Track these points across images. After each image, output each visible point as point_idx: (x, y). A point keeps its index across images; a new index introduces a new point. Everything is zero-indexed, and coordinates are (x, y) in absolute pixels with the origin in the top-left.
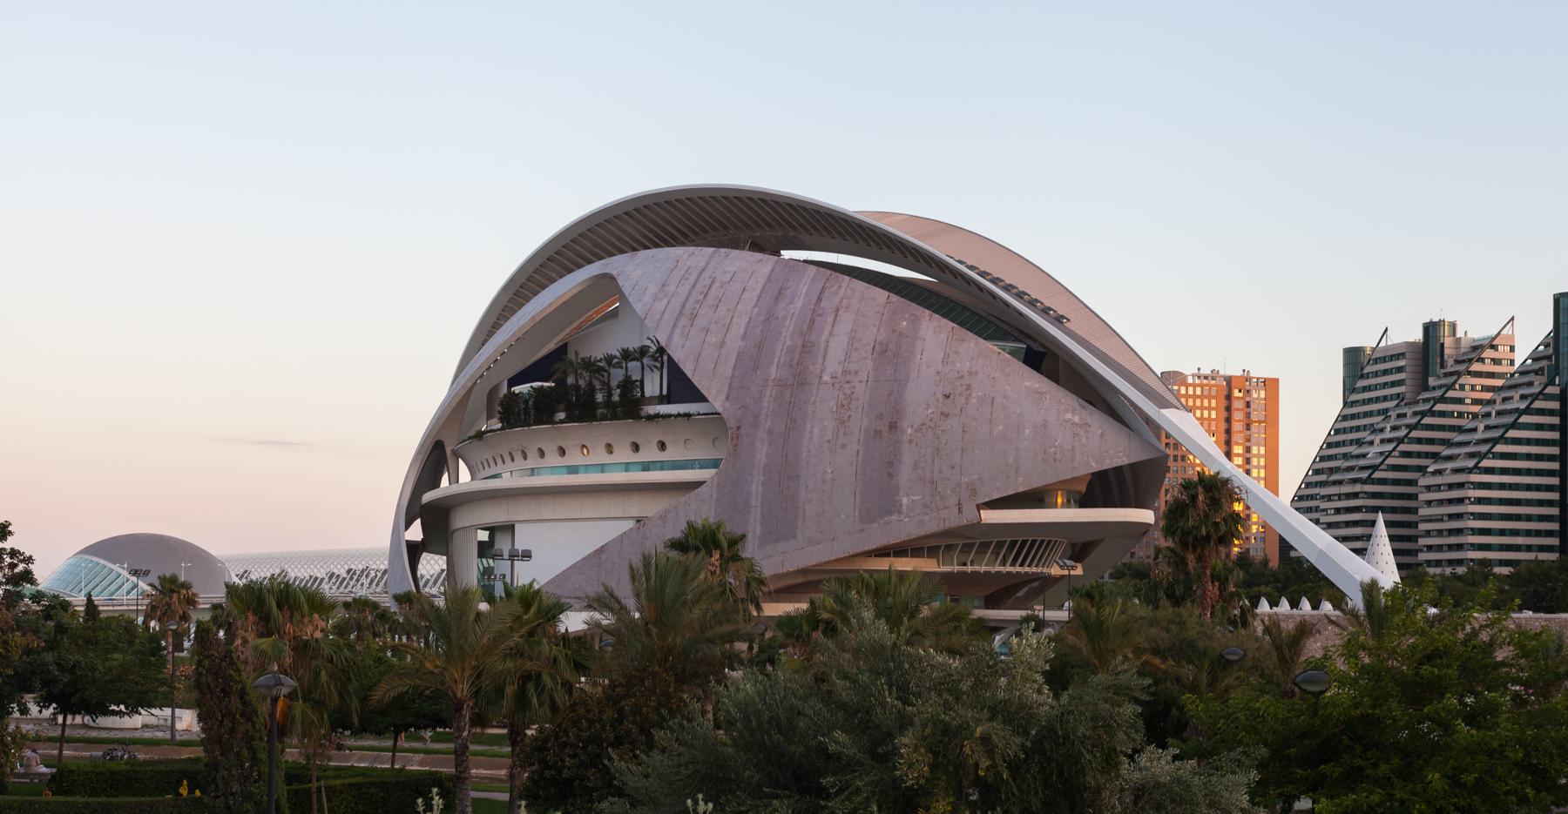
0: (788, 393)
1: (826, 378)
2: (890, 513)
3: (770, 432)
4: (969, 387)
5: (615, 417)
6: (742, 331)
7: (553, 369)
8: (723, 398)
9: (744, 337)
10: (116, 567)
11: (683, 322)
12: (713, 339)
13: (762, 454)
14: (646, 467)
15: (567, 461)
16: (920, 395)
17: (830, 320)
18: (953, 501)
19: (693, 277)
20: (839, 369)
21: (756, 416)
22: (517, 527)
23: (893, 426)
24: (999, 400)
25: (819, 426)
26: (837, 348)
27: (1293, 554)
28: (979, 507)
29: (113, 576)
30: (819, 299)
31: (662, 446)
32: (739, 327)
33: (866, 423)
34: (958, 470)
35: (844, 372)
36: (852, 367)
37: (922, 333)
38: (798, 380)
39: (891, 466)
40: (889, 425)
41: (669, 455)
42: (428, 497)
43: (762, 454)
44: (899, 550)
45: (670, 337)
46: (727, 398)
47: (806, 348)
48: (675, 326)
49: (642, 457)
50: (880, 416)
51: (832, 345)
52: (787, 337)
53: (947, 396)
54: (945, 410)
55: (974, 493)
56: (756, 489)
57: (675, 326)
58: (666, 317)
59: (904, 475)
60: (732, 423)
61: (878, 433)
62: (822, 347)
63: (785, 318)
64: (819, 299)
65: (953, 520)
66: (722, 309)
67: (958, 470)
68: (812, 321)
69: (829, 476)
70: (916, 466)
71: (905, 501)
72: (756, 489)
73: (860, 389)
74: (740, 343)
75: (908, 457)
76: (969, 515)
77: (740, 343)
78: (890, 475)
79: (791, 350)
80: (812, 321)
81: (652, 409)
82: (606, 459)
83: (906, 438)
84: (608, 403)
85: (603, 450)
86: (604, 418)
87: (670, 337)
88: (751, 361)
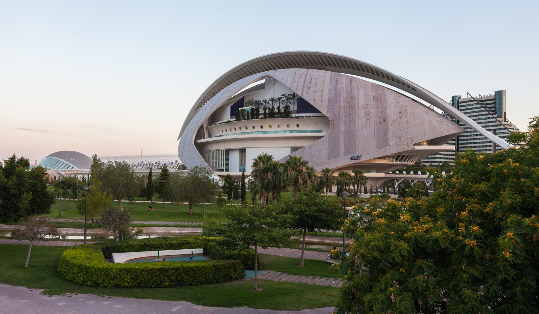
0: (348, 111)
1: (360, 106)
2: (386, 146)
3: (344, 122)
4: (406, 110)
5: (281, 117)
6: (328, 92)
7: (237, 102)
8: (326, 111)
9: (329, 94)
10: (61, 160)
11: (305, 89)
12: (318, 94)
13: (342, 128)
14: (292, 132)
15: (263, 130)
16: (392, 113)
17: (357, 89)
18: (406, 143)
19: (304, 77)
20: (364, 104)
21: (339, 117)
22: (247, 149)
23: (385, 121)
24: (416, 114)
25: (360, 121)
26: (361, 98)
27: (48, 295)
28: (414, 145)
29: (62, 163)
30: (351, 84)
31: (298, 126)
32: (326, 91)
33: (376, 120)
34: (407, 134)
35: (366, 105)
36: (368, 103)
37: (387, 94)
38: (351, 106)
39: (386, 132)
40: (384, 120)
41: (300, 128)
42: (200, 141)
43: (342, 128)
44: (384, 158)
45: (302, 93)
46: (328, 112)
47: (351, 98)
48: (303, 91)
49: (291, 129)
50: (380, 118)
51: (360, 97)
52: (344, 94)
53: (400, 112)
54: (401, 116)
55: (412, 140)
56: (342, 139)
57: (303, 91)
58: (299, 87)
59: (390, 135)
60: (331, 119)
61: (380, 123)
62: (356, 97)
63: (341, 89)
64: (351, 84)
65: (406, 148)
66: (318, 86)
67: (407, 134)
68: (351, 90)
69: (366, 135)
70: (394, 133)
71: (391, 143)
72: (342, 139)
73: (372, 110)
74: (328, 96)
75: (391, 130)
76: (411, 147)
77: (328, 96)
78: (386, 135)
79: (346, 98)
80: (351, 90)
81: (293, 115)
82: (278, 129)
83: (389, 124)
84: (279, 112)
85: (286, 126)
86: (278, 117)
87: (302, 93)
88: (334, 101)
